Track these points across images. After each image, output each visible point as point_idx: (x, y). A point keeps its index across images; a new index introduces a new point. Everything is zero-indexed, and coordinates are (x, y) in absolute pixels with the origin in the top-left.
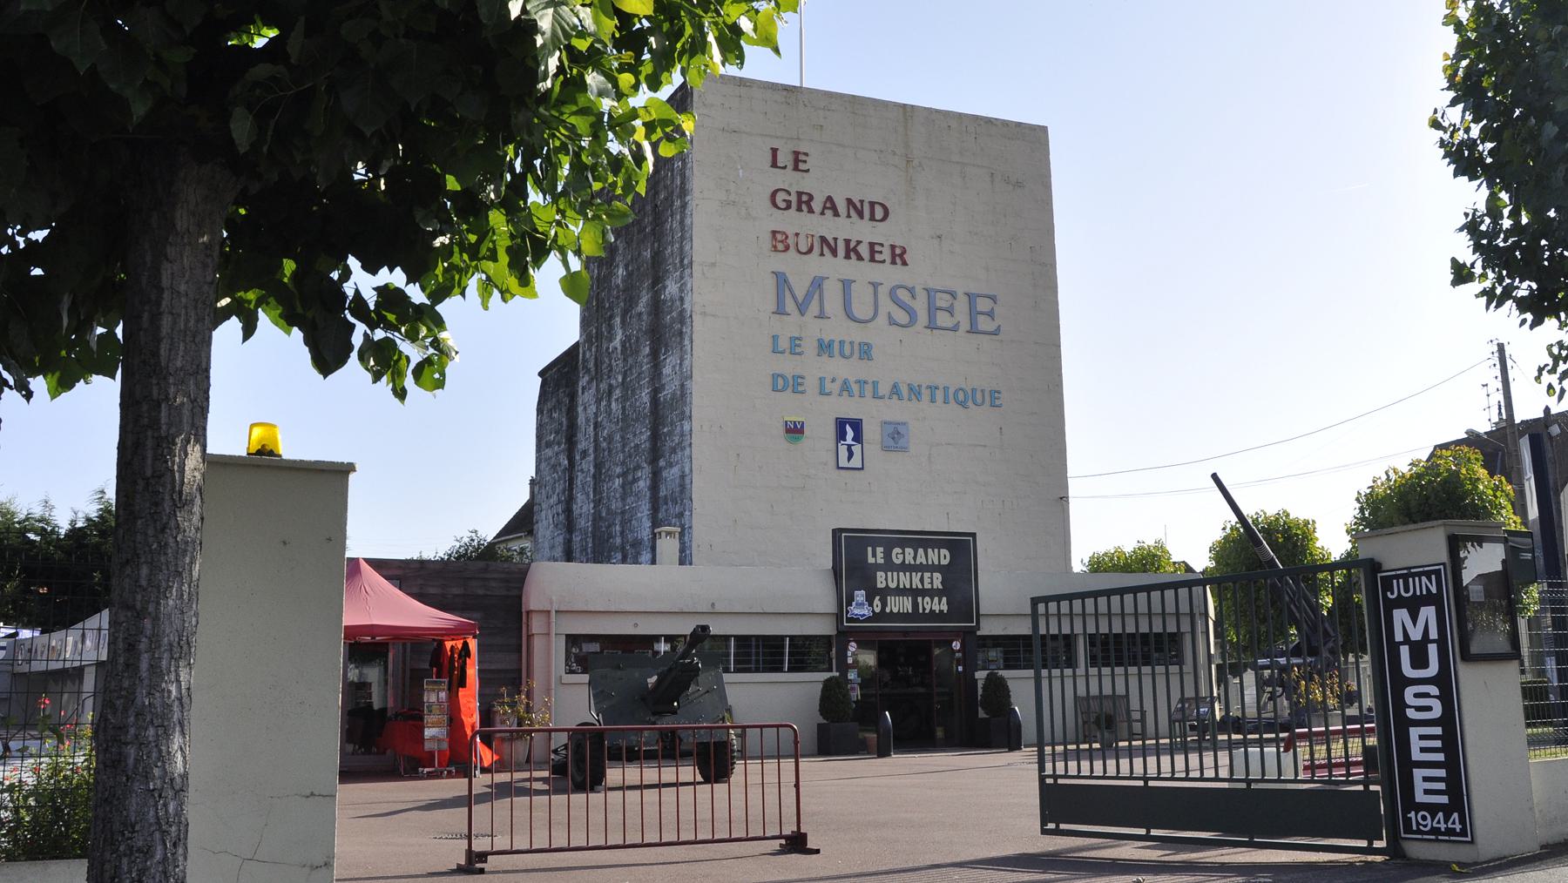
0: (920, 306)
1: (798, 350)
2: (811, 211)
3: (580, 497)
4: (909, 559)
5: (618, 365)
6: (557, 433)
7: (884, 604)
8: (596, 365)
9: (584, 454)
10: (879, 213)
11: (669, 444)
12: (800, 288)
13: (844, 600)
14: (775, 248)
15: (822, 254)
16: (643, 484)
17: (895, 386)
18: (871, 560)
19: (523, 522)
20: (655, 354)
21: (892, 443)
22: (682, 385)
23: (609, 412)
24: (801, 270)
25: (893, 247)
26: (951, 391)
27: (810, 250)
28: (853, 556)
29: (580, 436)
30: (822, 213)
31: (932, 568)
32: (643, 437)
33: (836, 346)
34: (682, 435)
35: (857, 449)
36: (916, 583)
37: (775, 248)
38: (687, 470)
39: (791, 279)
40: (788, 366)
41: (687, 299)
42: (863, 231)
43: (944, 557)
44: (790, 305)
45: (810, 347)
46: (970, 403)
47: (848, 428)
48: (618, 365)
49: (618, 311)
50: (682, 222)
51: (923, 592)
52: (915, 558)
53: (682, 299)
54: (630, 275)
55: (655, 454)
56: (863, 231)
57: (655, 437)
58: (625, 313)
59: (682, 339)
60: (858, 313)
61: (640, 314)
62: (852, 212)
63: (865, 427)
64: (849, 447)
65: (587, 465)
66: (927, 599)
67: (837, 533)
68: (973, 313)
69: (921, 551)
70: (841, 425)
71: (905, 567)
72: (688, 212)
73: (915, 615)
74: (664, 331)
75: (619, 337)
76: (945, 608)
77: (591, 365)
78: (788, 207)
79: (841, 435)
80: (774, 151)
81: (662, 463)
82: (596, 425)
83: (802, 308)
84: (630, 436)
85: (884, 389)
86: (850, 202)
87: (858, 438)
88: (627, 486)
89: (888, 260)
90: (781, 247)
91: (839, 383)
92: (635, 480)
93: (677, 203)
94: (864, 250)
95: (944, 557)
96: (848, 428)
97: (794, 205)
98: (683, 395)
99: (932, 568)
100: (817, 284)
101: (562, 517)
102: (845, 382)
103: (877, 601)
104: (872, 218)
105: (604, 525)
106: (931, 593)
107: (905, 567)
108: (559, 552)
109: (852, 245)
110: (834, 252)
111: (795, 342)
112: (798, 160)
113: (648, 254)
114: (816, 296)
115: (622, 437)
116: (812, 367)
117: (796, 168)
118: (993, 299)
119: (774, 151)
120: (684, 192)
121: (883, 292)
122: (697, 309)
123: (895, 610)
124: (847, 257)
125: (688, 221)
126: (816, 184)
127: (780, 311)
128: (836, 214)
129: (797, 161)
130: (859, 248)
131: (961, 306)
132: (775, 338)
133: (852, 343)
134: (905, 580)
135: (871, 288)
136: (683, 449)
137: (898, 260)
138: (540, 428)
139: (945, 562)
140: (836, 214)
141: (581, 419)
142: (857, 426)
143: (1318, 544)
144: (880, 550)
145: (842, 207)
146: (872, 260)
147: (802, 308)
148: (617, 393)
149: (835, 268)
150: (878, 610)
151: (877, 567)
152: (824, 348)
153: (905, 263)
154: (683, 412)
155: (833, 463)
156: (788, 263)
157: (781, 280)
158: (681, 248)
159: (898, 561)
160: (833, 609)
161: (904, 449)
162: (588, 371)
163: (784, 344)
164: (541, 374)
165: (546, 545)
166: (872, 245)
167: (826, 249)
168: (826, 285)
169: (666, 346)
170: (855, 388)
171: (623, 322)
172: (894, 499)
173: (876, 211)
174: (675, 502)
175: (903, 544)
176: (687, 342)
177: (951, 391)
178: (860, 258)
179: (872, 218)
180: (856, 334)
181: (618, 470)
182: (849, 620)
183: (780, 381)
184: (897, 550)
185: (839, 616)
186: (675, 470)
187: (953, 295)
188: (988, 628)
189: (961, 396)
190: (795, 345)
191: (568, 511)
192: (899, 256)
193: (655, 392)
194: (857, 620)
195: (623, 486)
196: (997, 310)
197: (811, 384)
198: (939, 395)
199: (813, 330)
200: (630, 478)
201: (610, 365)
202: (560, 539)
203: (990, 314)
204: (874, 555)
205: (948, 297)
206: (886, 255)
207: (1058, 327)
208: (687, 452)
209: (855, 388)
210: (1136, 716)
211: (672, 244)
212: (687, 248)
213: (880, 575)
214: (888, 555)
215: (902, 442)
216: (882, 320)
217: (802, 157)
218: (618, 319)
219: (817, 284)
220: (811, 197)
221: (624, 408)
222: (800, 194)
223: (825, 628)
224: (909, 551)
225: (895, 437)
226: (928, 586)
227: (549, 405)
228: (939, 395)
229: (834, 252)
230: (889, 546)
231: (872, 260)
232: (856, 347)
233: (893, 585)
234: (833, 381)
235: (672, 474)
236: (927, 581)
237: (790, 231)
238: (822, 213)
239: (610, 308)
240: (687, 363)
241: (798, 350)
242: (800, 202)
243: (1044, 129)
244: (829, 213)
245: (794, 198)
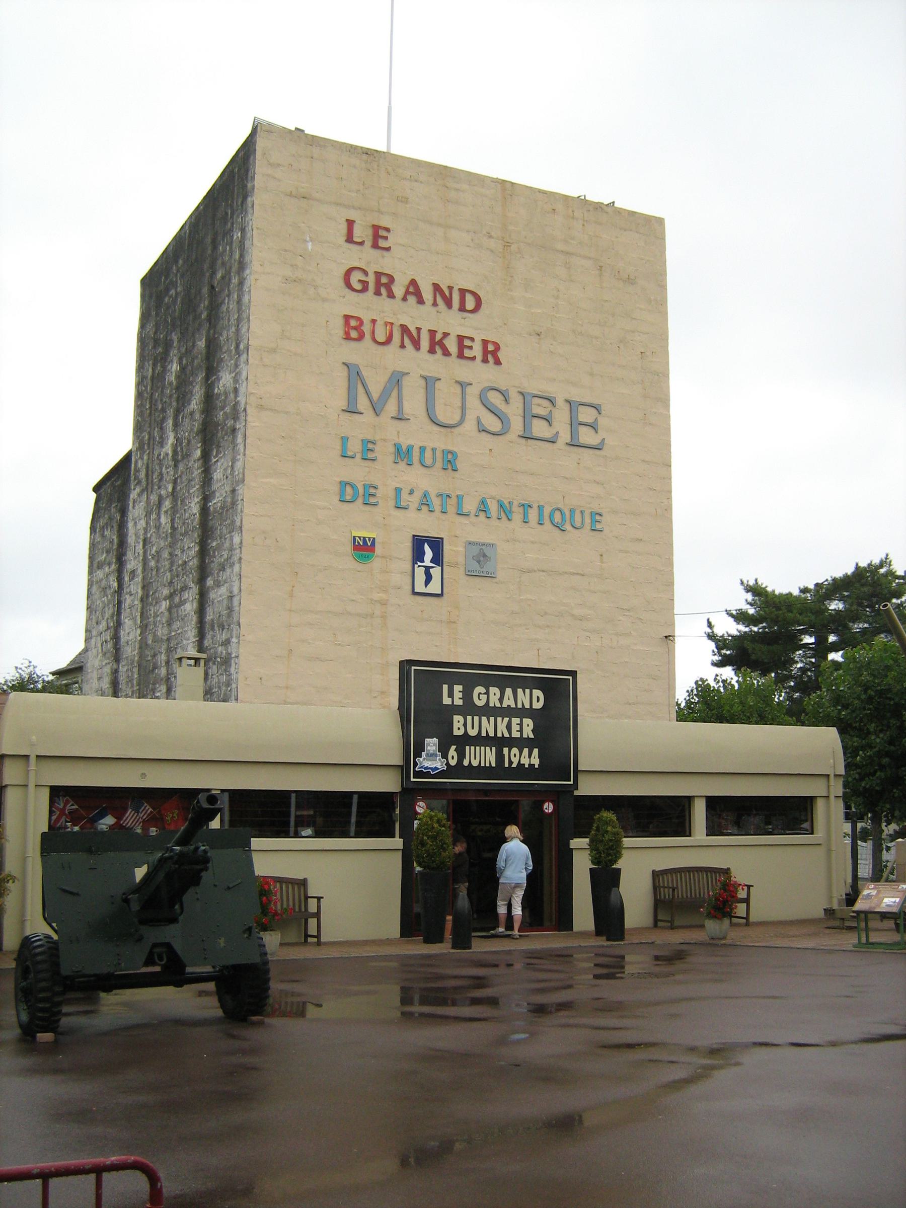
0: (514, 411)
1: (370, 455)
2: (391, 295)
3: (127, 623)
4: (494, 701)
5: (169, 473)
6: (108, 552)
7: (461, 755)
8: (147, 475)
9: (133, 573)
10: (470, 303)
11: (218, 560)
12: (376, 383)
13: (412, 748)
14: (348, 337)
15: (403, 346)
16: (190, 608)
17: (483, 502)
18: (447, 701)
19: (85, 650)
20: (206, 456)
21: (476, 566)
22: (233, 491)
23: (158, 527)
24: (379, 363)
25: (485, 343)
26: (547, 511)
28: (426, 693)
29: (130, 555)
30: (404, 299)
31: (522, 713)
32: (190, 549)
33: (416, 453)
34: (231, 549)
35: (436, 572)
36: (502, 730)
37: (348, 337)
38: (236, 590)
39: (365, 373)
40: (358, 472)
41: (242, 390)
42: (452, 323)
43: (537, 699)
44: (363, 403)
45: (384, 453)
46: (568, 527)
47: (427, 548)
48: (169, 473)
49: (170, 412)
50: (239, 302)
51: (510, 742)
52: (501, 700)
53: (236, 390)
54: (183, 369)
55: (203, 573)
56: (452, 323)
57: (204, 552)
58: (178, 412)
59: (235, 437)
60: (441, 417)
61: (192, 413)
62: (439, 300)
63: (447, 547)
64: (428, 569)
65: (135, 588)
66: (515, 750)
67: (405, 665)
68: (575, 424)
69: (509, 691)
70: (418, 543)
71: (487, 711)
72: (246, 289)
73: (499, 770)
74: (215, 431)
75: (171, 439)
76: (536, 761)
77: (142, 475)
78: (365, 289)
79: (418, 556)
80: (350, 223)
81: (210, 582)
82: (145, 541)
83: (377, 410)
84: (178, 552)
85: (470, 505)
86: (437, 288)
87: (437, 559)
89: (479, 357)
91: (418, 495)
92: (182, 603)
93: (235, 281)
94: (452, 345)
95: (537, 699)
96: (427, 548)
97: (372, 286)
98: (234, 503)
99: (522, 713)
100: (397, 380)
101: (110, 645)
102: (425, 495)
103: (452, 752)
104: (462, 309)
105: (149, 653)
106: (521, 743)
107: (487, 711)
108: (106, 684)
109: (438, 337)
110: (417, 345)
111: (368, 446)
112: (378, 235)
113: (202, 344)
114: (395, 393)
115: (171, 554)
116: (389, 476)
117: (375, 246)
118: (597, 408)
119: (350, 223)
120: (242, 266)
121: (473, 392)
122: (252, 400)
123: (475, 763)
124: (432, 351)
125: (246, 299)
126: (400, 265)
127: (351, 410)
128: (421, 301)
131: (561, 416)
132: (344, 440)
133: (434, 450)
134: (488, 726)
135: (458, 389)
136: (232, 565)
138: (93, 546)
139: (538, 705)
140: (421, 301)
141: (131, 539)
142: (437, 545)
144: (458, 688)
145: (427, 294)
146: (461, 355)
147: (377, 410)
148: (167, 504)
149: (418, 363)
150: (453, 763)
151: (454, 709)
152: (402, 454)
153: (498, 362)
154: (233, 522)
155: (410, 588)
156: (361, 353)
157: (354, 375)
158: (238, 331)
159: (480, 703)
160: (398, 760)
161: (491, 576)
162: (139, 483)
163: (355, 447)
164: (96, 489)
165: (95, 675)
166: (461, 339)
167: (407, 341)
168: (406, 382)
169: (218, 446)
170: (436, 503)
171: (176, 425)
172: (477, 630)
173: (468, 301)
174: (222, 627)
175: (488, 682)
176: (240, 439)
177: (547, 511)
178: (446, 353)
179: (462, 309)
180: (437, 440)
181: (166, 592)
182: (418, 774)
183: (349, 490)
184: (480, 689)
185: (404, 769)
186: (223, 590)
187: (552, 401)
188: (588, 788)
189: (557, 517)
190: (368, 449)
191: (116, 638)
192: (491, 353)
193: (206, 499)
195: (170, 610)
196: (603, 422)
197: (385, 492)
198: (533, 515)
199: (391, 433)
200: (177, 599)
201: (161, 474)
202: (107, 670)
203: (593, 427)
204: (451, 695)
205: (546, 403)
206: (477, 351)
207: (669, 445)
208: (236, 568)
209: (436, 503)
211: (228, 327)
212: (244, 330)
213: (458, 720)
214: (467, 695)
215: (488, 567)
216: (470, 425)
217: (382, 233)
218: (170, 422)
219: (397, 380)
220: (391, 279)
221: (173, 521)
222: (378, 275)
223: (388, 783)
224: (494, 690)
225: (481, 561)
226: (516, 734)
227: (102, 522)
228: (533, 515)
229: (417, 345)
230: (469, 685)
231: (461, 355)
232: (439, 454)
233: (473, 733)
234: (411, 492)
235: (218, 595)
236: (515, 728)
237: (366, 318)
238: (404, 299)
239: (163, 410)
240: (239, 465)
241: (370, 455)
243: (650, 229)
244: (412, 299)
245: (371, 279)
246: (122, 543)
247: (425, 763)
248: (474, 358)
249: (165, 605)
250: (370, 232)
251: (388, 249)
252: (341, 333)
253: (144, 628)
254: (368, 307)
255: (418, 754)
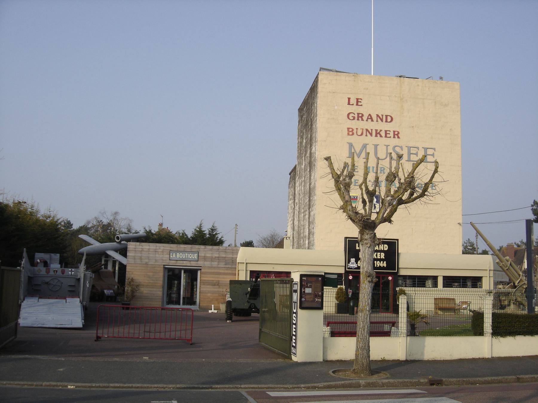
2: (362, 120)
10: (389, 119)
16: (307, 216)
20: (310, 171)
25: (394, 132)
27: (362, 134)
31: (381, 251)
37: (348, 134)
39: (354, 144)
42: (383, 126)
43: (386, 247)
56: (383, 126)
66: (378, 262)
76: (385, 265)
80: (349, 99)
86: (378, 116)
88: (304, 216)
90: (351, 133)
94: (383, 134)
95: (386, 247)
99: (381, 251)
100: (365, 146)
104: (386, 121)
106: (380, 260)
109: (378, 132)
110: (371, 134)
113: (309, 136)
118: (434, 149)
119: (349, 99)
124: (376, 136)
126: (364, 110)
128: (372, 121)
129: (357, 102)
130: (381, 133)
137: (396, 136)
139: (386, 249)
140: (372, 121)
143: (337, 302)
149: (371, 140)
153: (398, 137)
156: (353, 139)
157: (351, 145)
166: (386, 131)
173: (388, 119)
178: (381, 136)
179: (386, 121)
187: (418, 148)
188: (402, 272)
191: (293, 223)
192: (396, 135)
193: (310, 184)
194: (352, 269)
196: (436, 154)
203: (433, 155)
206: (392, 134)
210: (214, 386)
219: (365, 146)
220: (363, 115)
222: (358, 114)
223: (342, 271)
229: (371, 134)
231: (386, 136)
235: (312, 214)
236: (378, 255)
238: (367, 121)
242: (358, 117)
244: (370, 120)
245: (356, 116)
246: (295, 194)
247: (351, 265)
248: (390, 137)
249: (303, 214)
250: (356, 100)
251: (361, 105)
252: (347, 133)
253: (299, 221)
254: (355, 124)
255: (349, 263)
